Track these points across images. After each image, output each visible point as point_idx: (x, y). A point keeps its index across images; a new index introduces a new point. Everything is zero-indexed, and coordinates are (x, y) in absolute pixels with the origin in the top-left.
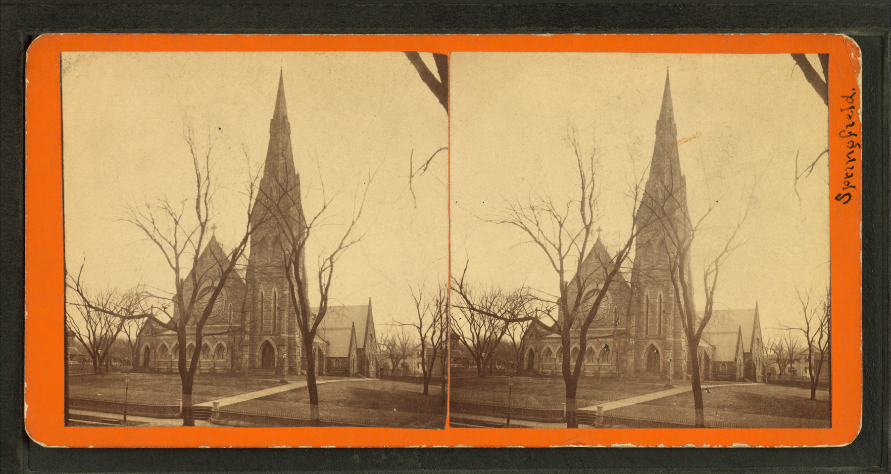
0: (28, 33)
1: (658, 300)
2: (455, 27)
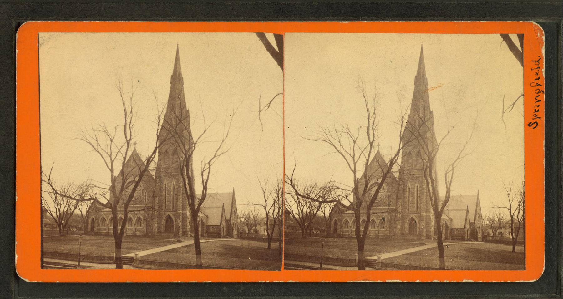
0: (17, 21)
2: (287, 17)
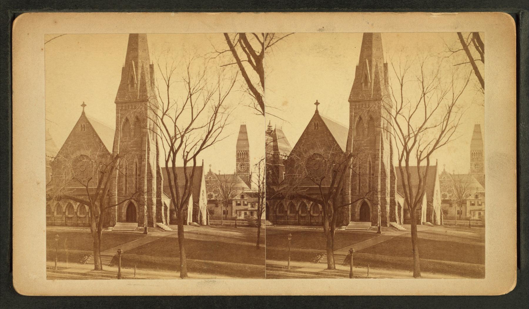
0: (13, 12)
1: (368, 165)
2: (264, 8)
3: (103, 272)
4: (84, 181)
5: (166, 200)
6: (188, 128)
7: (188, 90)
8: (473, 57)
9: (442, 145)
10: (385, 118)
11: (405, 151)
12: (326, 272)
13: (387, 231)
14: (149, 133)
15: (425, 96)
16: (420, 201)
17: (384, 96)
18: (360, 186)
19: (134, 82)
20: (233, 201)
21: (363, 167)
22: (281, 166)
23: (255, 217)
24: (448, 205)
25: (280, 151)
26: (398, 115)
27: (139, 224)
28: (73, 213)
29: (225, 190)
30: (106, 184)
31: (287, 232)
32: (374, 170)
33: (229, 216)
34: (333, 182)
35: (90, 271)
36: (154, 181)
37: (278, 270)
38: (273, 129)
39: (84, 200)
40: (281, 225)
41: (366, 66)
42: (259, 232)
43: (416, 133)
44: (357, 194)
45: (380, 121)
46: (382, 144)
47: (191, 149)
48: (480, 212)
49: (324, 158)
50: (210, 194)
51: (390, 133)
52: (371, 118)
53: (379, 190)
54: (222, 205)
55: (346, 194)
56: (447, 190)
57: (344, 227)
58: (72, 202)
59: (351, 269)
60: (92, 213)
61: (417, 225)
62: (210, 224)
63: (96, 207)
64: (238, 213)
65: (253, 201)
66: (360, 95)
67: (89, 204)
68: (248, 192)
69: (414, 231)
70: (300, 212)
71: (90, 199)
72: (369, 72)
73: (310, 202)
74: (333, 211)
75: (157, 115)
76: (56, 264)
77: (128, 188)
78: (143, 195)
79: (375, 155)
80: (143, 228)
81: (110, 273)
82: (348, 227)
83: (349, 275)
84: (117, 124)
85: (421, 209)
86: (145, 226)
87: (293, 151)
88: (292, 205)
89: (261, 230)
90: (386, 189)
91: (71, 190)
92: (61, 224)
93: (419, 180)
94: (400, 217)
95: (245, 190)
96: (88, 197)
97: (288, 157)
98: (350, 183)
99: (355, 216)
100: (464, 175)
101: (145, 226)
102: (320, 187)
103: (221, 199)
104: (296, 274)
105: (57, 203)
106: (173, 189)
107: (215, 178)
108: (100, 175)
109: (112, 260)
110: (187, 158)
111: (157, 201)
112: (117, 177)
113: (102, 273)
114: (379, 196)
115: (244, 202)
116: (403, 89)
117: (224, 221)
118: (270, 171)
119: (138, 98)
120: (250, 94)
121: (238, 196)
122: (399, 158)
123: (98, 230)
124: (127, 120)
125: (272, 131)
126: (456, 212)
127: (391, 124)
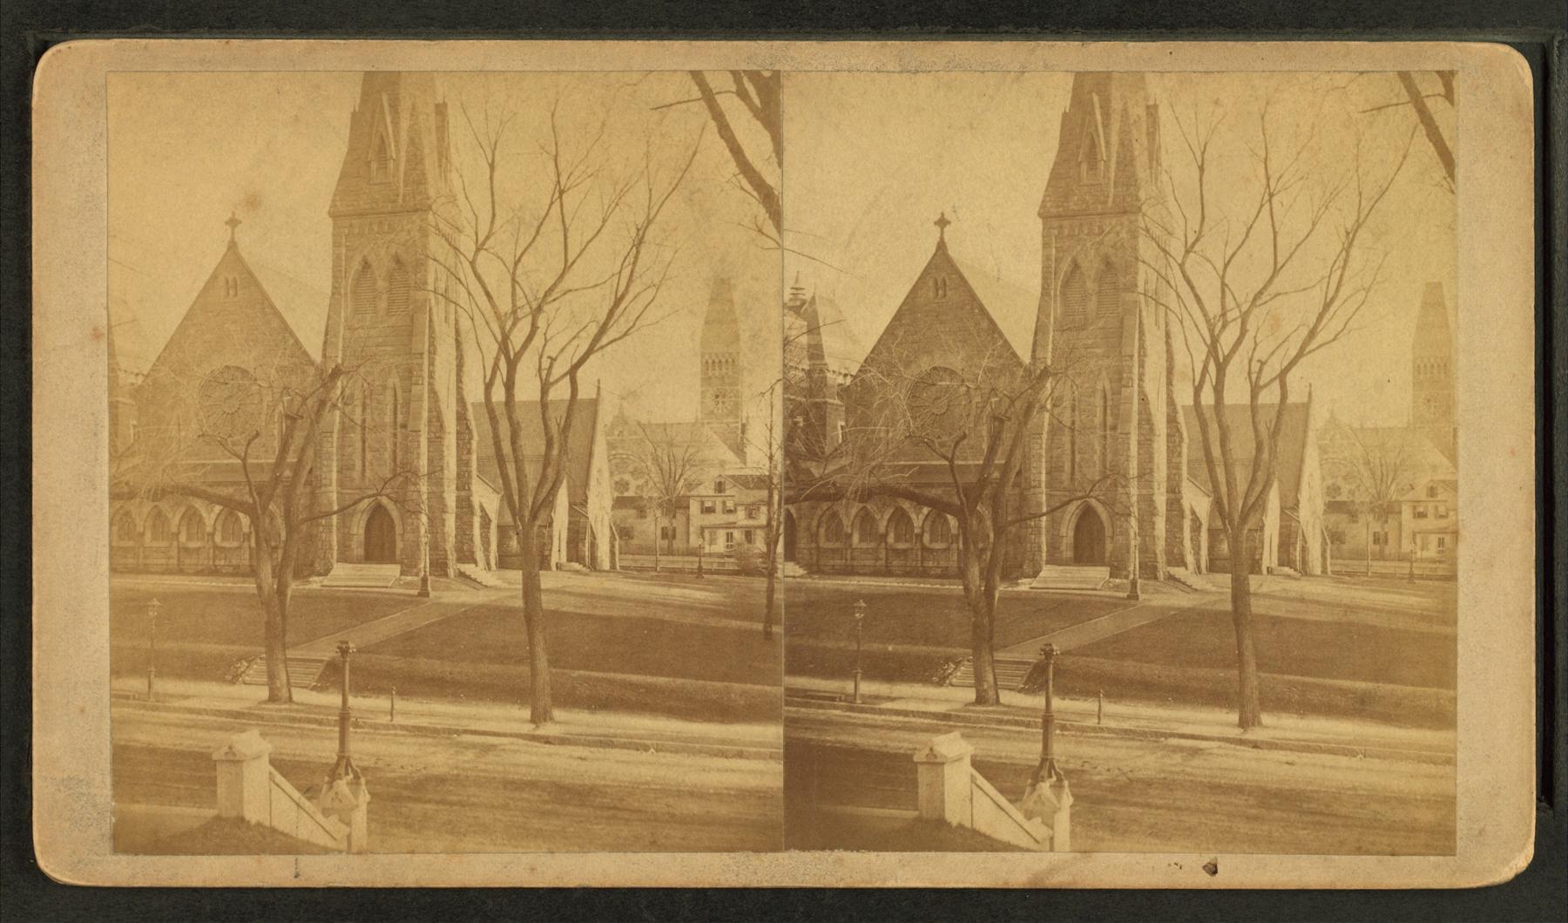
3: (295, 707)
4: (234, 444)
5: (486, 498)
6: (551, 290)
7: (555, 179)
8: (712, 86)
9: (615, 340)
10: (1150, 266)
11: (503, 357)
12: (973, 711)
13: (1157, 592)
14: (433, 301)
15: (1275, 200)
16: (1259, 505)
17: (1148, 201)
18: (364, 458)
19: (1099, 157)
20: (691, 501)
21: (1082, 407)
22: (833, 404)
23: (760, 545)
24: (633, 512)
25: (827, 360)
26: (483, 253)
27: (405, 568)
28: (911, 537)
29: (666, 467)
30: (303, 450)
31: (855, 596)
32: (1116, 416)
33: (678, 544)
34: (992, 450)
35: (958, 706)
36: (451, 440)
37: (821, 706)
38: (808, 297)
39: (237, 497)
40: (833, 574)
41: (383, 112)
42: (771, 591)
43: (1244, 308)
44: (357, 482)
45: (1136, 273)
46: (1140, 339)
47: (562, 350)
48: (729, 531)
49: (963, 381)
50: (622, 479)
51: (1167, 307)
52: (1108, 264)
53: (1133, 470)
54: (659, 513)
55: (324, 482)
56: (631, 468)
57: (1024, 580)
58: (906, 505)
59: (345, 701)
60: (261, 534)
61: (541, 572)
62: (1333, 572)
63: (272, 519)
64: (1419, 541)
65: (750, 500)
66: (1076, 198)
67: (250, 510)
68: (737, 473)
69: (531, 588)
70: (183, 538)
71: (255, 494)
72: (390, 129)
73: (922, 508)
74: (992, 535)
75: (456, 249)
76: (149, 687)
77: (372, 464)
78: (416, 484)
79: (1120, 373)
80: (416, 578)
81: (1024, 713)
82: (1039, 582)
83: (1040, 720)
84: (1045, 279)
85: (1262, 528)
86: (1131, 577)
87: (868, 361)
88: (866, 519)
89: (776, 586)
90: (445, 466)
91: (195, 467)
92: (165, 567)
93: (544, 442)
94: (487, 550)
95: (727, 467)
96: (248, 488)
97: (855, 377)
98: (335, 450)
99: (1059, 548)
100: (679, 424)
101: (1131, 577)
102: (952, 466)
103: (655, 495)
104: (879, 719)
105: (862, 509)
106: (509, 466)
107: (635, 433)
108: (284, 425)
109: (324, 672)
110: (549, 374)
111: (459, 500)
112: (336, 431)
113: (291, 710)
114: (1134, 491)
115: (1436, 508)
116: (1204, 180)
117: (663, 558)
118: (800, 419)
119: (1110, 204)
120: (742, 188)
121: (707, 484)
122: (485, 377)
123: (986, 586)
124: (366, 265)
125: (804, 302)
126: (1371, 539)
127: (1168, 282)
